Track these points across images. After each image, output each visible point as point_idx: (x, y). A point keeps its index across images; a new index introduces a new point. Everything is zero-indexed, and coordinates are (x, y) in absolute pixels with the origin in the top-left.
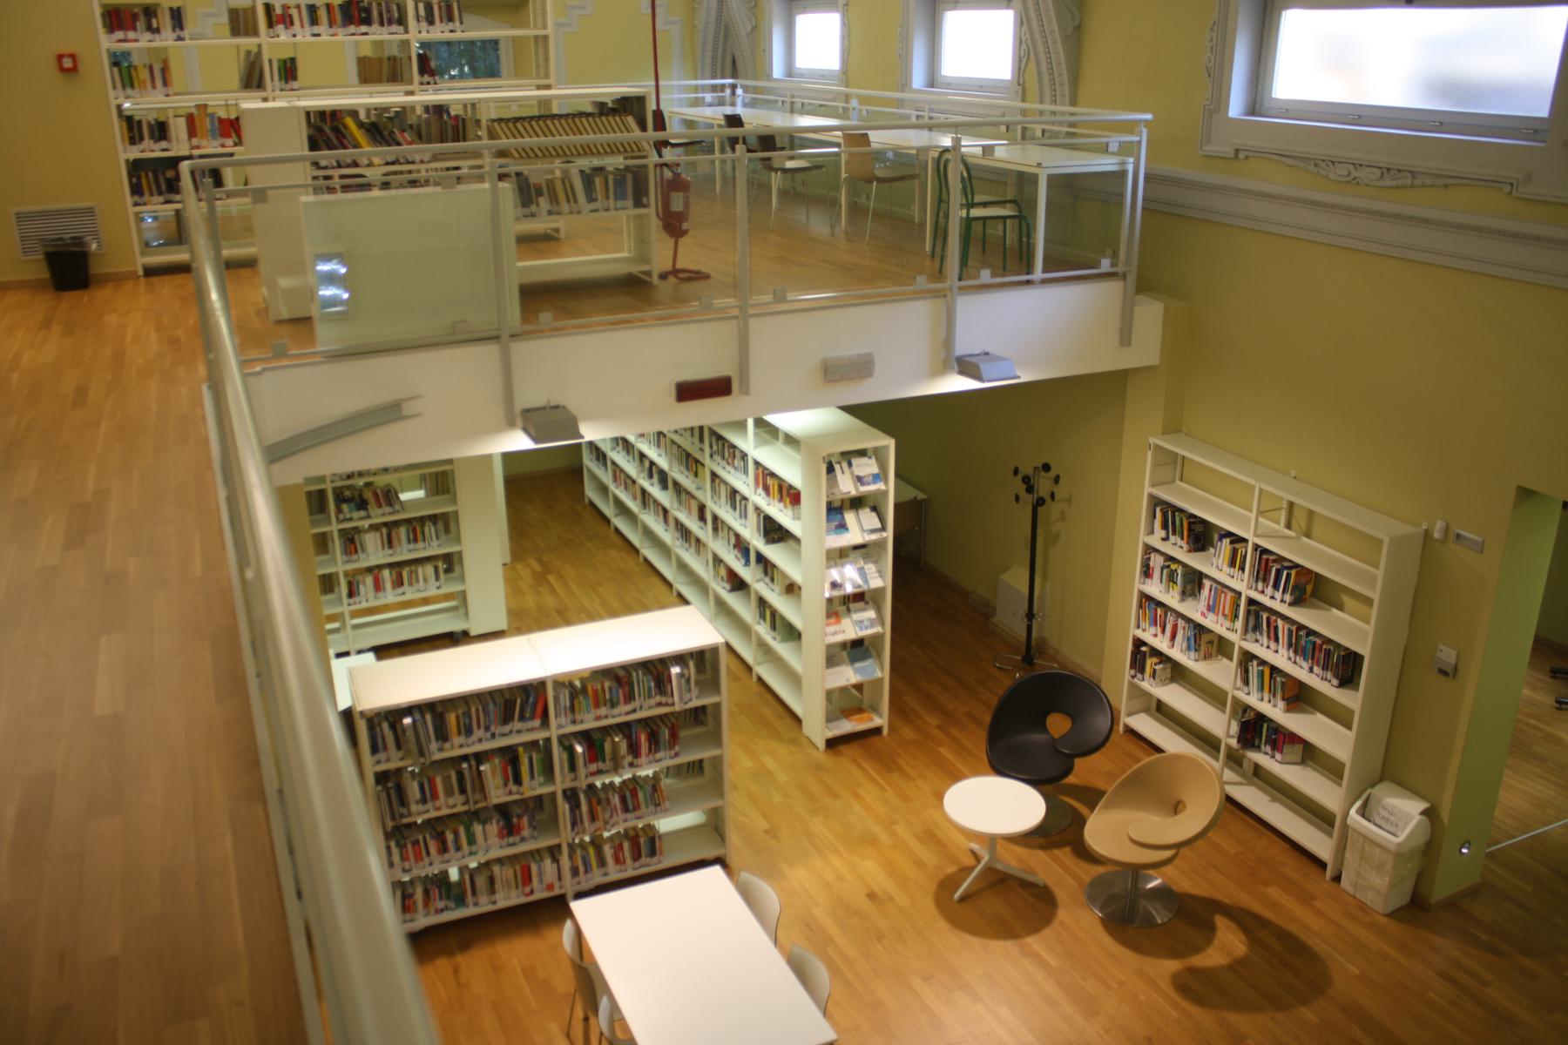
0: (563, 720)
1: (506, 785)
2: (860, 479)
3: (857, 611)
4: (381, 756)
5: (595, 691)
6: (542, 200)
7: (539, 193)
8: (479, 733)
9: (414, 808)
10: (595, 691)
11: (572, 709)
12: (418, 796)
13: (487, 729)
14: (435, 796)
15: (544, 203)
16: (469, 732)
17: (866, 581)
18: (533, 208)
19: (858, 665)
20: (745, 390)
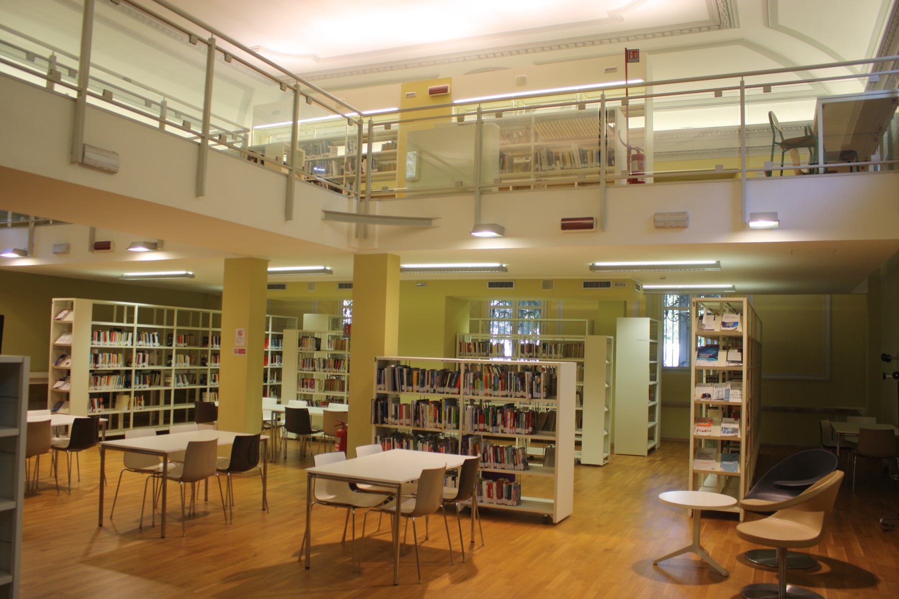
0: (467, 390)
1: (435, 421)
2: (724, 324)
3: (726, 422)
4: (382, 386)
5: (486, 377)
6: (558, 162)
7: (557, 158)
8: (427, 387)
9: (390, 418)
10: (486, 377)
11: (474, 387)
12: (393, 413)
13: (432, 386)
14: (401, 417)
15: (559, 165)
16: (423, 385)
17: (728, 398)
18: (553, 166)
19: (725, 463)
20: (603, 229)
